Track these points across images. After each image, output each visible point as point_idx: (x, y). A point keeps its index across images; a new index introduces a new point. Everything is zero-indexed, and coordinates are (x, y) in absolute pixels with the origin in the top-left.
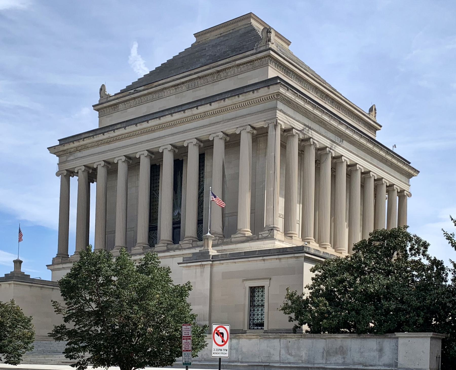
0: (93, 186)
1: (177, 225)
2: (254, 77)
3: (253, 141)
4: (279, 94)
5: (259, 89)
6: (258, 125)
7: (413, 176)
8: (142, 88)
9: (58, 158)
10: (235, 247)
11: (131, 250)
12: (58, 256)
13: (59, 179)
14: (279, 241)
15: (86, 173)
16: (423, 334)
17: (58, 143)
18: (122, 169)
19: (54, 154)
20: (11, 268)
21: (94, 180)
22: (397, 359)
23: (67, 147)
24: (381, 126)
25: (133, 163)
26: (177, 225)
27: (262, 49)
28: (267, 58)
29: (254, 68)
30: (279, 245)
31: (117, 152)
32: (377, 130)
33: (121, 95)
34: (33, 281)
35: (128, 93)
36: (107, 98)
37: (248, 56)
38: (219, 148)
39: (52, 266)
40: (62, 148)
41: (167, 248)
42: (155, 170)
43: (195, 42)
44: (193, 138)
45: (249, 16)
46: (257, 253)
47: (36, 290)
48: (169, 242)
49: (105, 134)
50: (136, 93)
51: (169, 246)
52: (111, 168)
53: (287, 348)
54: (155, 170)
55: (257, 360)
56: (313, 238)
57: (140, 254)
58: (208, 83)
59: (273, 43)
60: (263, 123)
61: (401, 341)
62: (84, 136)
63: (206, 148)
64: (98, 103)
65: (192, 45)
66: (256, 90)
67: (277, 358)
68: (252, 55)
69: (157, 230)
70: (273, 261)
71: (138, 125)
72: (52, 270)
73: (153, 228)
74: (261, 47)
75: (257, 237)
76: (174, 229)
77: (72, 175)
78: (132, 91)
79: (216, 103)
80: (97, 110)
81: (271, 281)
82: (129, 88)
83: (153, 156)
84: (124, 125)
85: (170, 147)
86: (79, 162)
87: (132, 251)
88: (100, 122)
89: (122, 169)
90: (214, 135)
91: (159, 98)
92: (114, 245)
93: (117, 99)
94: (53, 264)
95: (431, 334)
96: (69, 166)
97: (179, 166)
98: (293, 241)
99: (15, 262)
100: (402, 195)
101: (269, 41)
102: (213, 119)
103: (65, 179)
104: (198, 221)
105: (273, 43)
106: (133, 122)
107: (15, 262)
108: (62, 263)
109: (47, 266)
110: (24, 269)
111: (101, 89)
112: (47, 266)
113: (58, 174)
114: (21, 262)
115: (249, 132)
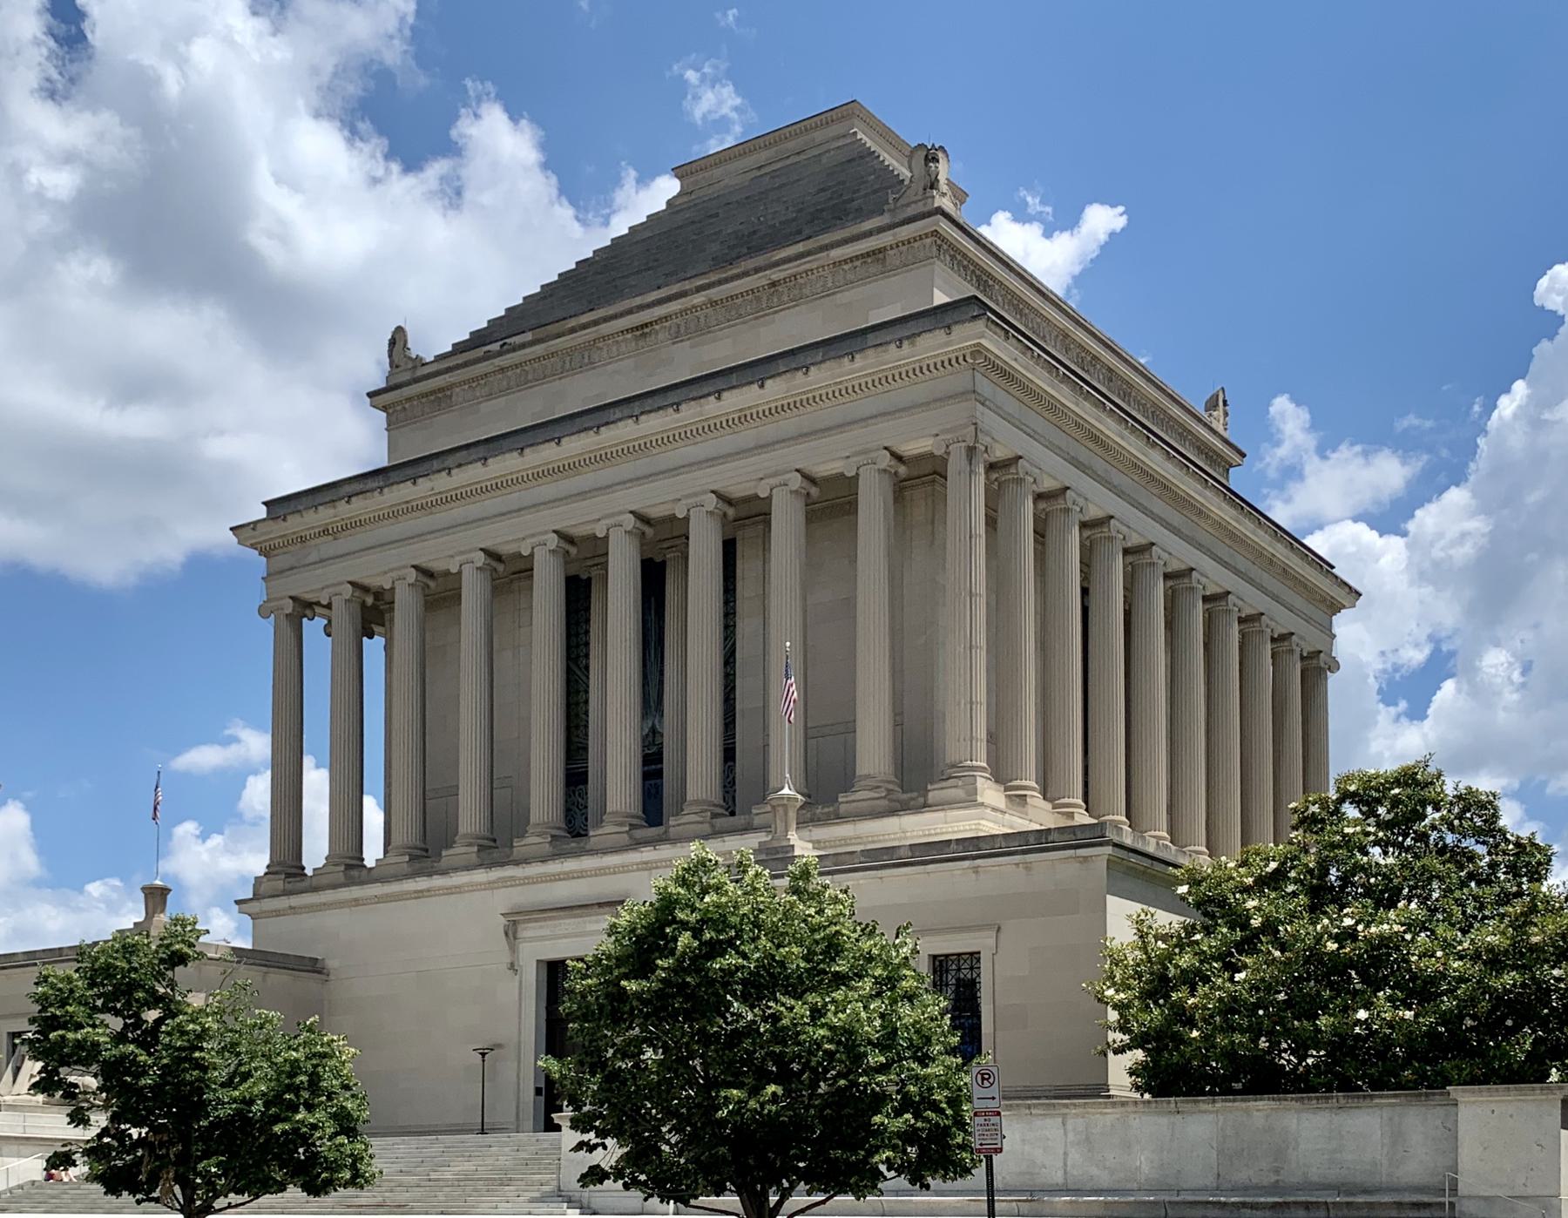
0: (374, 648)
2: (887, 300)
3: (896, 500)
4: (978, 351)
5: (919, 334)
6: (910, 448)
7: (1344, 607)
8: (528, 336)
9: (264, 559)
10: (852, 834)
11: (512, 847)
12: (271, 871)
13: (267, 627)
14: (994, 809)
17: (262, 513)
18: (473, 592)
19: (252, 546)
21: (376, 629)
23: (294, 524)
24: (1243, 455)
25: (509, 573)
27: (910, 212)
28: (928, 241)
29: (886, 272)
30: (990, 826)
32: (1231, 466)
33: (460, 359)
35: (480, 352)
36: (415, 367)
37: (869, 234)
38: (786, 521)
39: (255, 904)
40: (279, 528)
41: (713, 826)
42: (580, 596)
43: (679, 195)
44: (704, 492)
45: (849, 111)
46: (953, 846)
48: (635, 821)
49: (420, 480)
50: (508, 352)
52: (439, 592)
53: (1087, 1141)
54: (580, 596)
56: (1080, 802)
59: (944, 194)
60: (930, 441)
61: (1464, 1113)
62: (348, 489)
63: (745, 520)
64: (383, 385)
65: (669, 203)
66: (908, 338)
68: (881, 230)
69: (586, 782)
71: (527, 451)
72: (254, 917)
73: (576, 778)
74: (908, 205)
75: (921, 800)
76: (646, 776)
77: (308, 612)
78: (496, 347)
79: (778, 379)
80: (384, 409)
81: (1002, 936)
83: (573, 550)
84: (481, 452)
85: (630, 522)
87: (930, 795)
88: (392, 447)
89: (473, 592)
90: (773, 481)
92: (684, 799)
93: (449, 370)
94: (257, 896)
96: (306, 585)
97: (654, 581)
98: (1030, 810)
101: (932, 187)
102: (769, 430)
103: (288, 631)
105: (944, 194)
108: (287, 893)
109: (237, 902)
111: (392, 343)
112: (237, 902)
113: (263, 612)
115: (885, 471)
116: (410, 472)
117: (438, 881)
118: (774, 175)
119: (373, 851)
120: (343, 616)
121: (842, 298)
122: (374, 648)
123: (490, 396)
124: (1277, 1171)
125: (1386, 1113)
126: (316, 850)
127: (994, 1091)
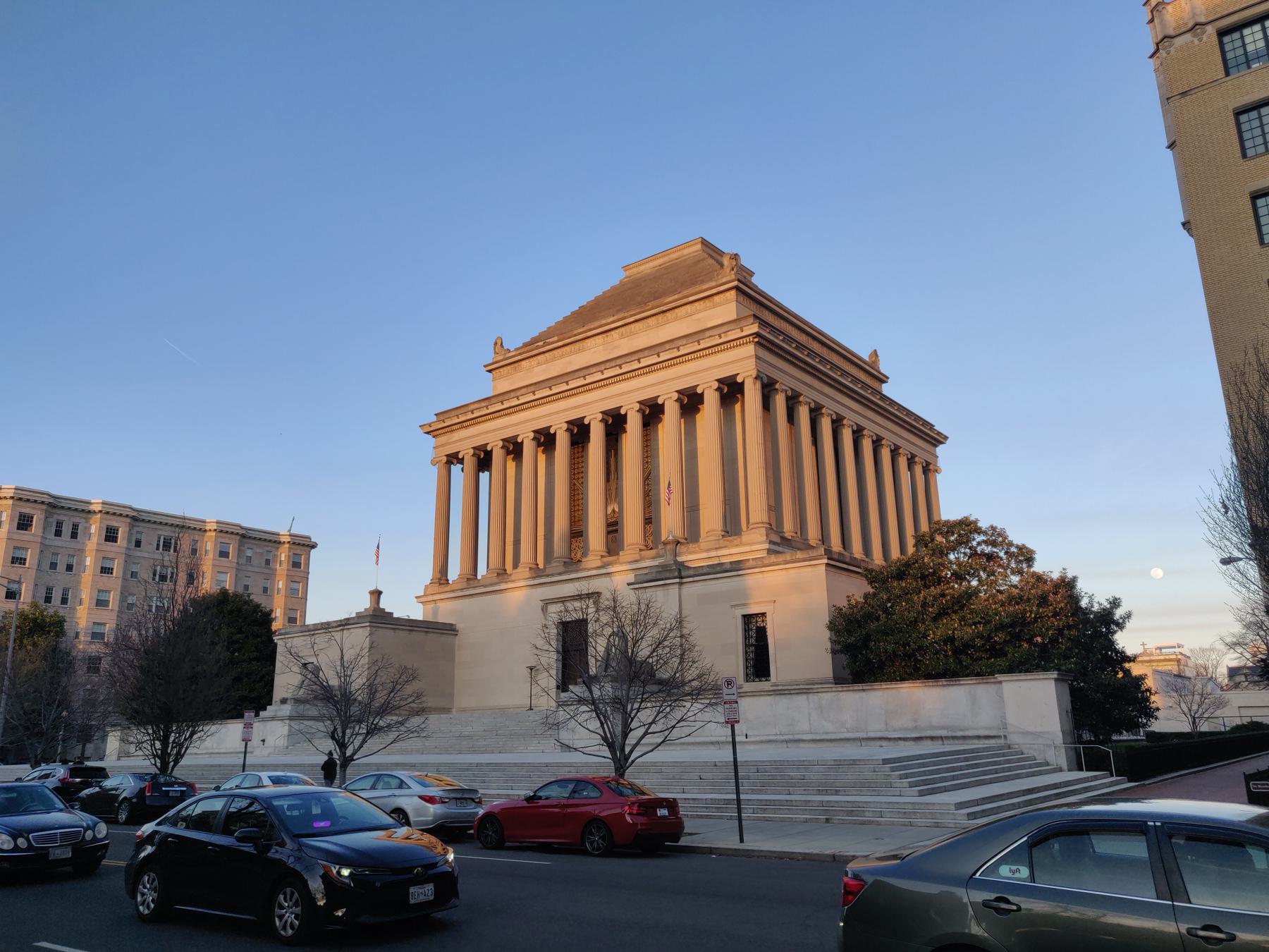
1: (613, 528)
13: (435, 470)
15: (474, 459)
16: (1041, 675)
20: (364, 604)
22: (1004, 717)
25: (545, 439)
26: (613, 528)
27: (724, 280)
31: (523, 425)
34: (400, 622)
47: (402, 635)
51: (605, 560)
52: (514, 448)
55: (774, 731)
57: (760, 543)
58: (650, 327)
64: (735, 317)
67: (806, 727)
70: (792, 571)
82: (534, 341)
86: (465, 441)
88: (495, 388)
91: (580, 351)
95: (1055, 675)
99: (372, 593)
100: (929, 469)
104: (609, 525)
106: (544, 385)
107: (372, 593)
110: (386, 604)
113: (434, 463)
114: (380, 593)
116: (501, 398)
117: (510, 585)
118: (666, 268)
119: (482, 570)
120: (470, 462)
121: (694, 317)
122: (484, 476)
123: (539, 364)
124: (915, 721)
125: (968, 687)
126: (454, 573)
127: (734, 690)
